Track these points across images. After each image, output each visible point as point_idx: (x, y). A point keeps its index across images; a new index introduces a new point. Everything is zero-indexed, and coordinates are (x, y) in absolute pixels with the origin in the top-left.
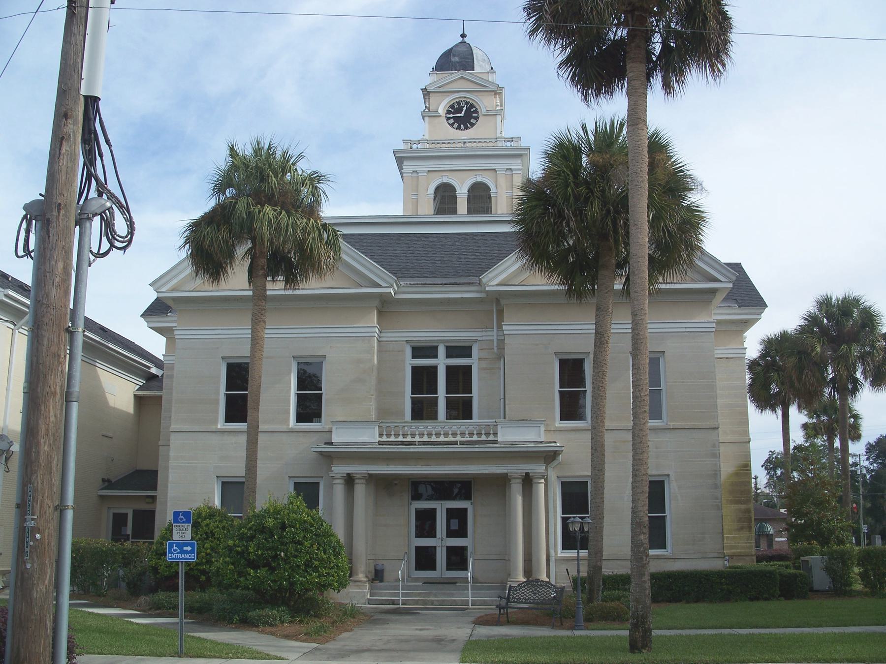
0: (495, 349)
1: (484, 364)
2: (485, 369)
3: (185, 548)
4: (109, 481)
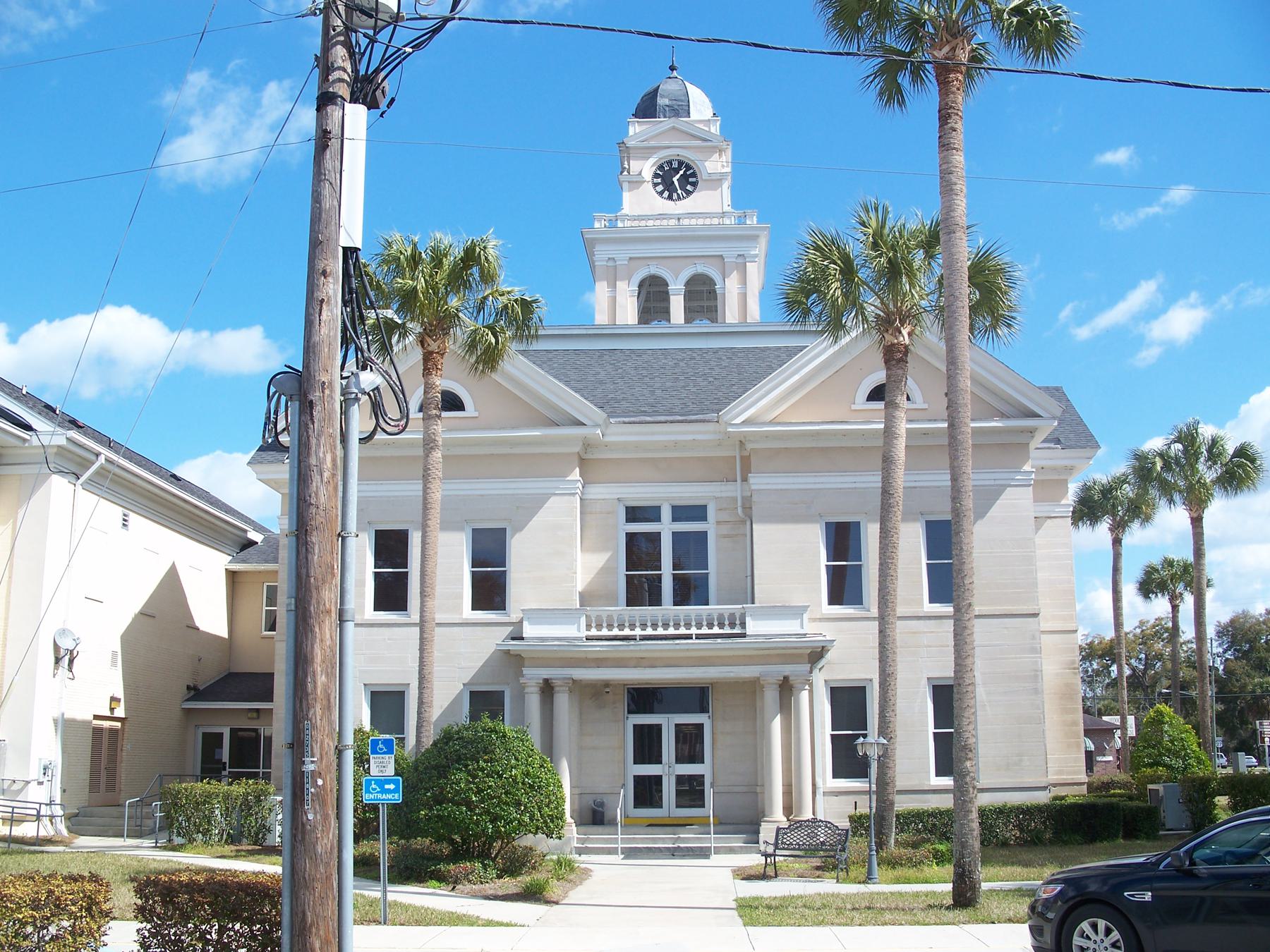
0: (740, 510)
1: (725, 530)
2: (725, 536)
3: (387, 787)
4: (195, 688)
